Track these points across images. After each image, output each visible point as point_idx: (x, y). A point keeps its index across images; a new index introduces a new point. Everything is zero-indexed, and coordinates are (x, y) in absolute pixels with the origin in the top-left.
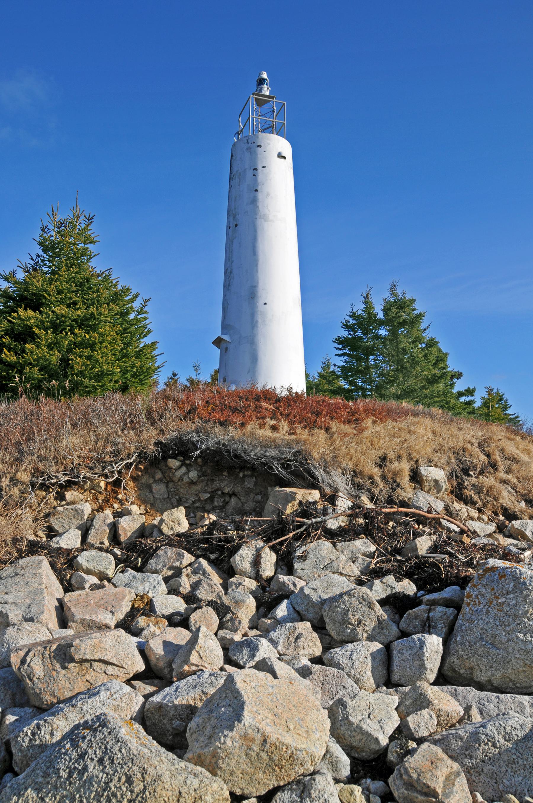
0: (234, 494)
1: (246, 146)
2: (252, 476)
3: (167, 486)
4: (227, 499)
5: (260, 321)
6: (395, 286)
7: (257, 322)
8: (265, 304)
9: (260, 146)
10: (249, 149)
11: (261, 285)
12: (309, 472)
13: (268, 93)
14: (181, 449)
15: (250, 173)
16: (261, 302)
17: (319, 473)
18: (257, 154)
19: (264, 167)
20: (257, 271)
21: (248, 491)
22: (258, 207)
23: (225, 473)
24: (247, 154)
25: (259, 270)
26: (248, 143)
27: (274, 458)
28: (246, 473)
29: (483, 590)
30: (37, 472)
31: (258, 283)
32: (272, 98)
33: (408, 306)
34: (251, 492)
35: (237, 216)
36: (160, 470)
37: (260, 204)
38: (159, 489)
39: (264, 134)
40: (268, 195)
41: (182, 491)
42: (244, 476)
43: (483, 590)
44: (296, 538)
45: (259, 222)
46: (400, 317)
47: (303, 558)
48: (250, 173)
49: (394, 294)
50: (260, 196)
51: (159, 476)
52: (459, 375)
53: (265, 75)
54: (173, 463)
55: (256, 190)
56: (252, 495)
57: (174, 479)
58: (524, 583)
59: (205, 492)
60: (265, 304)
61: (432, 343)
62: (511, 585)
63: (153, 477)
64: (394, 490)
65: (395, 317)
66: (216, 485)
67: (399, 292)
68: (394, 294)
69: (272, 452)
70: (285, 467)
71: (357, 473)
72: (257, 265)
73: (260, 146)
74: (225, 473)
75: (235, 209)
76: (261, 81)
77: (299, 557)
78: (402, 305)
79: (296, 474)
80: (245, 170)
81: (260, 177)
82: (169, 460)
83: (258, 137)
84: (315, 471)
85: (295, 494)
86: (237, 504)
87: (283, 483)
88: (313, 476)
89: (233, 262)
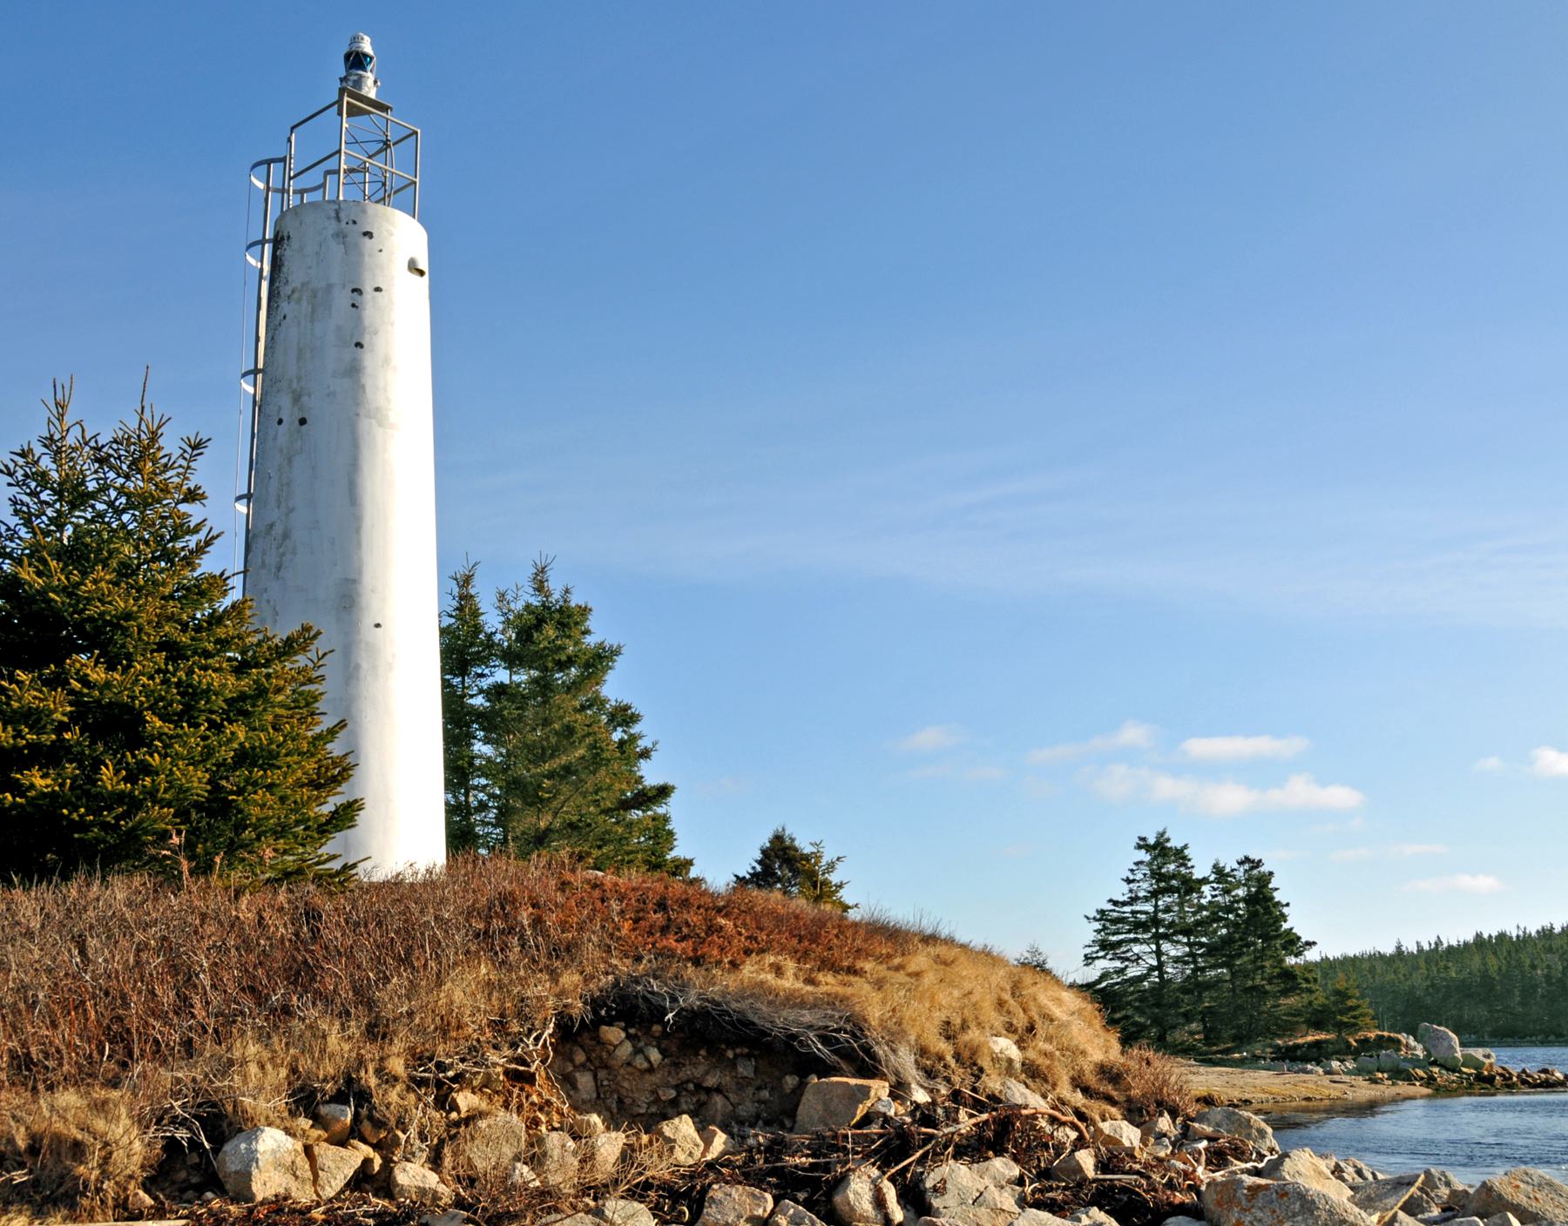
0: (718, 1090)
1: (332, 226)
2: (748, 1056)
3: (595, 1077)
4: (703, 1097)
5: (364, 665)
6: (543, 570)
7: (357, 667)
8: (378, 626)
9: (368, 234)
10: (341, 236)
11: (368, 579)
12: (867, 1050)
13: (372, 95)
14: (628, 1007)
15: (342, 298)
16: (367, 622)
17: (881, 1051)
18: (360, 254)
19: (378, 289)
20: (359, 545)
21: (742, 1083)
22: (363, 387)
23: (703, 1052)
24: (336, 249)
25: (364, 543)
26: (338, 219)
27: (810, 1027)
28: (738, 1051)
29: (1260, 1214)
30: (418, 1058)
31: (360, 571)
32: (384, 108)
33: (577, 624)
34: (749, 1084)
35: (305, 399)
36: (581, 1047)
37: (367, 381)
38: (585, 1080)
39: (380, 206)
40: (387, 360)
41: (626, 1084)
42: (736, 1056)
43: (1260, 1214)
44: (922, 1161)
45: (364, 424)
46: (562, 648)
47: (940, 1190)
48: (342, 298)
49: (540, 587)
50: (369, 361)
51: (580, 1057)
52: (1310, 944)
53: (367, 46)
54: (613, 1034)
55: (359, 345)
56: (750, 1090)
57: (613, 1062)
58: (1313, 1202)
59: (668, 1085)
60: (378, 626)
61: (623, 716)
62: (1298, 1205)
63: (572, 1061)
64: (978, 1078)
65: (550, 650)
66: (687, 1072)
67: (555, 587)
68: (540, 587)
69: (807, 1017)
70: (825, 1040)
71: (923, 1052)
72: (358, 530)
73: (368, 234)
74: (703, 1052)
75: (299, 379)
76: (356, 61)
77: (935, 1189)
78: (569, 619)
79: (847, 1055)
80: (329, 287)
81: (369, 313)
82: (604, 1028)
83: (364, 211)
84: (876, 1048)
85: (869, 1088)
86: (724, 1106)
87: (826, 1070)
88: (873, 1056)
89: (292, 510)
